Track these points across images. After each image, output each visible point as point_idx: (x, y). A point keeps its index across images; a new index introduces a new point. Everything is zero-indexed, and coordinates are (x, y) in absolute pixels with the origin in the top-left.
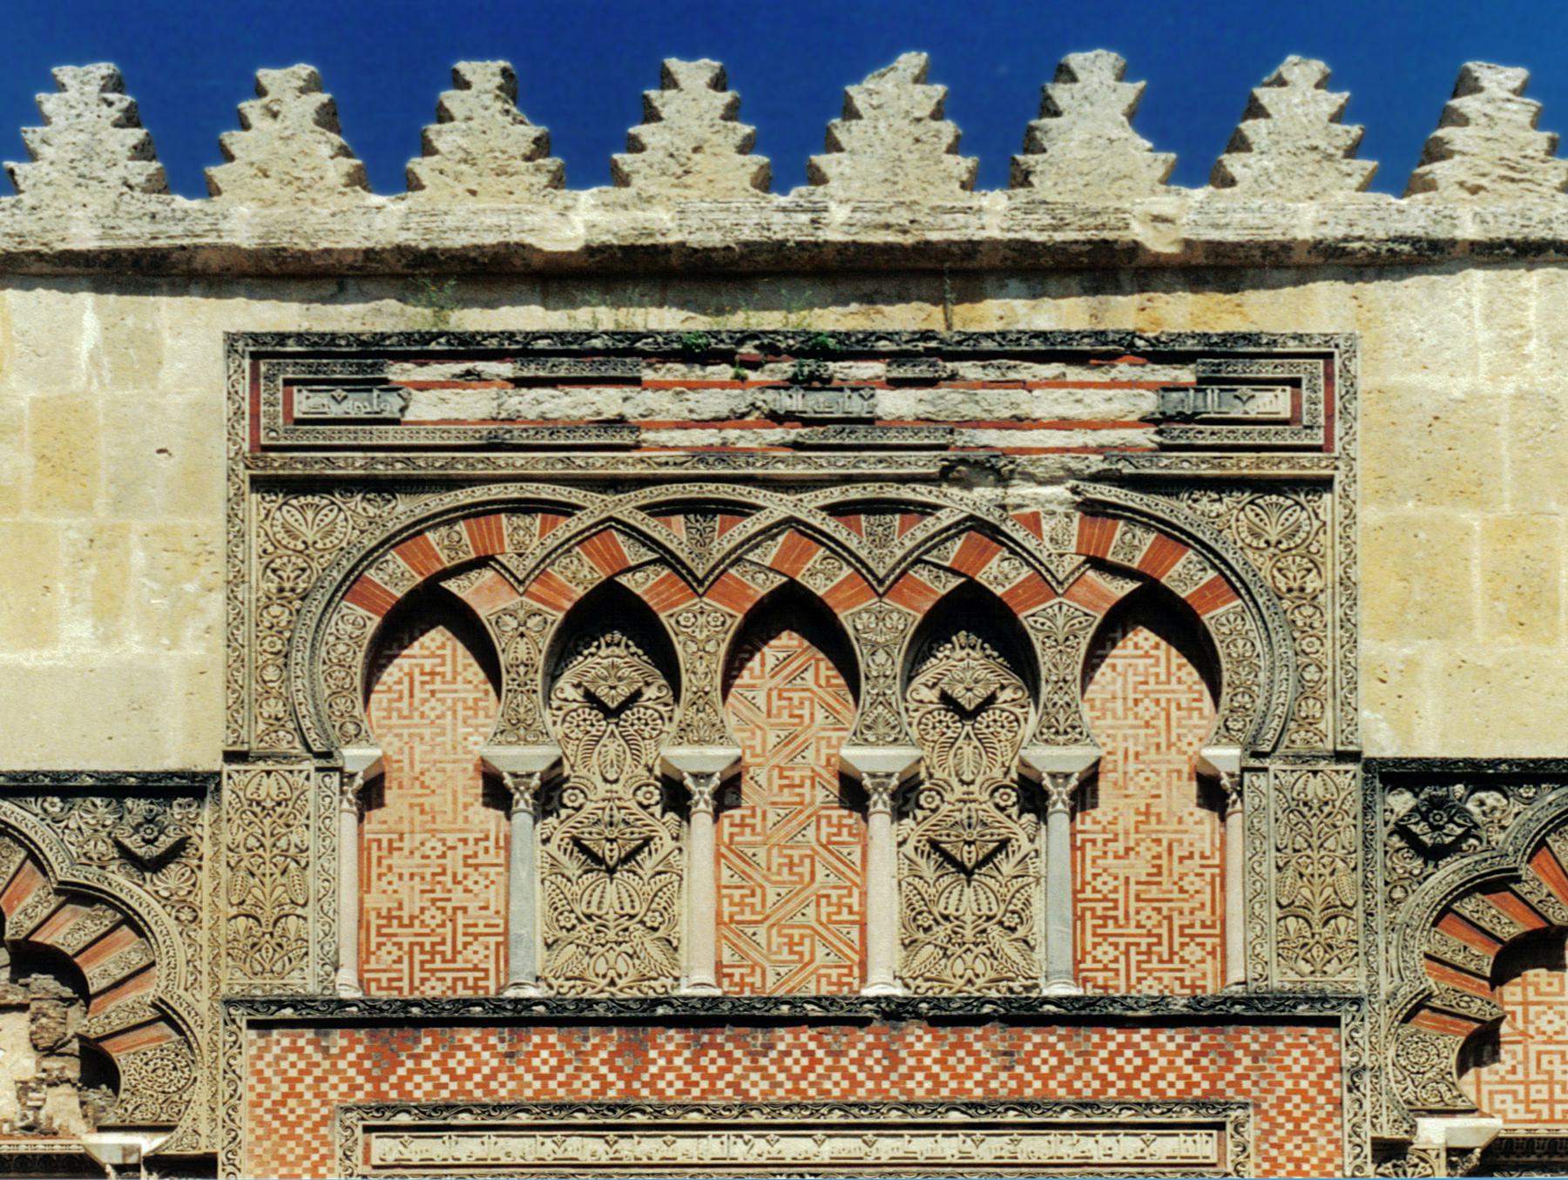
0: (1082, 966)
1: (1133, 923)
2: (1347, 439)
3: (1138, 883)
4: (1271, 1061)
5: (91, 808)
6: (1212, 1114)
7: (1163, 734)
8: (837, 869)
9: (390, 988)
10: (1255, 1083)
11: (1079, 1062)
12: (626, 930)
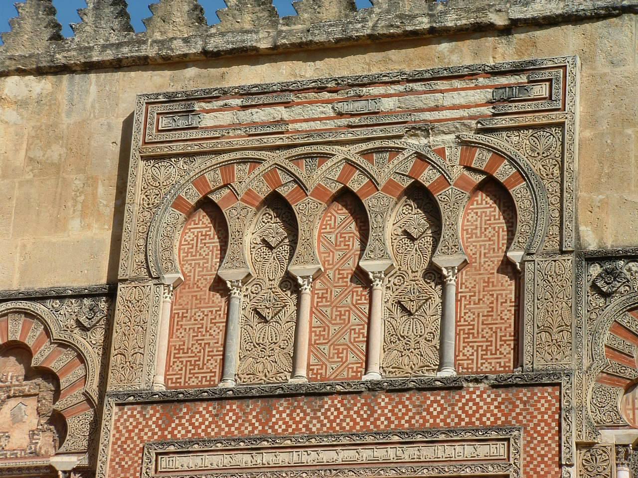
0: (458, 358)
1: (480, 336)
2: (571, 104)
3: (483, 316)
4: (532, 406)
5: (70, 305)
6: (503, 433)
7: (496, 244)
8: (359, 316)
9: (176, 383)
10: (525, 417)
11: (449, 409)
12: (273, 350)
